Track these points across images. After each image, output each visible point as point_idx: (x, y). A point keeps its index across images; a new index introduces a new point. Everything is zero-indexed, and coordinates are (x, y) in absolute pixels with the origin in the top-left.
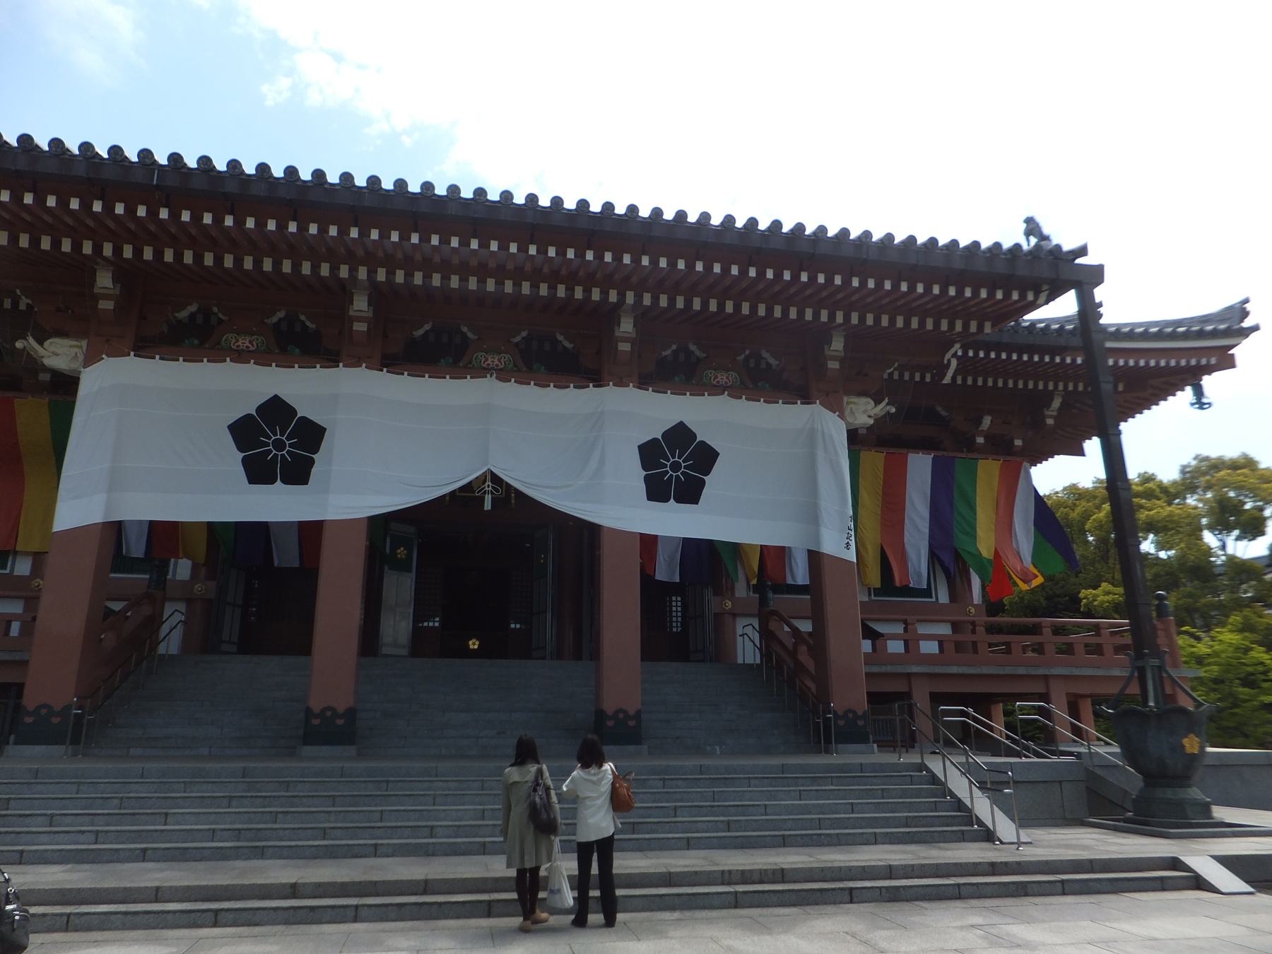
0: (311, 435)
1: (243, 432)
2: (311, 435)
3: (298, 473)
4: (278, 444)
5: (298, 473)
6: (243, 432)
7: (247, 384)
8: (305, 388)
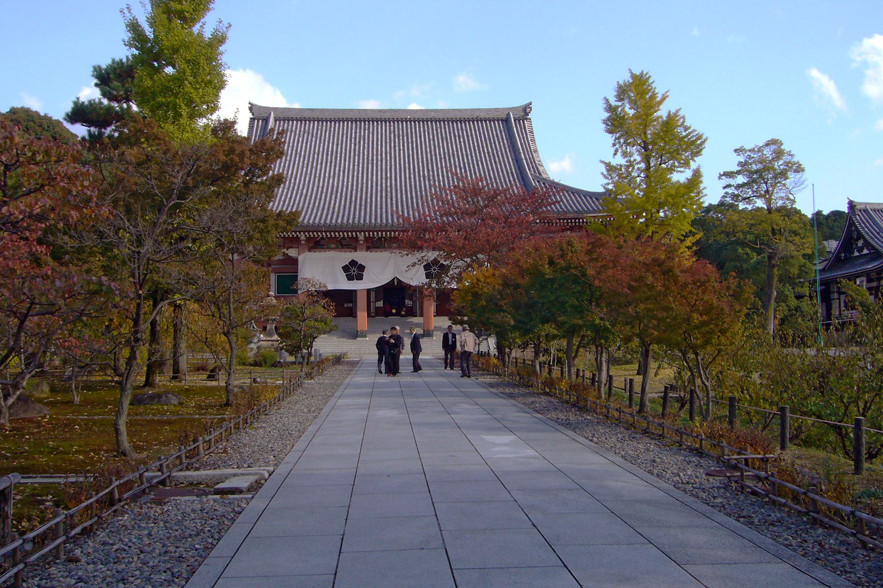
0: (362, 268)
1: (346, 269)
2: (362, 268)
3: (360, 277)
4: (354, 271)
5: (360, 277)
6: (346, 269)
7: (347, 257)
8: (360, 256)
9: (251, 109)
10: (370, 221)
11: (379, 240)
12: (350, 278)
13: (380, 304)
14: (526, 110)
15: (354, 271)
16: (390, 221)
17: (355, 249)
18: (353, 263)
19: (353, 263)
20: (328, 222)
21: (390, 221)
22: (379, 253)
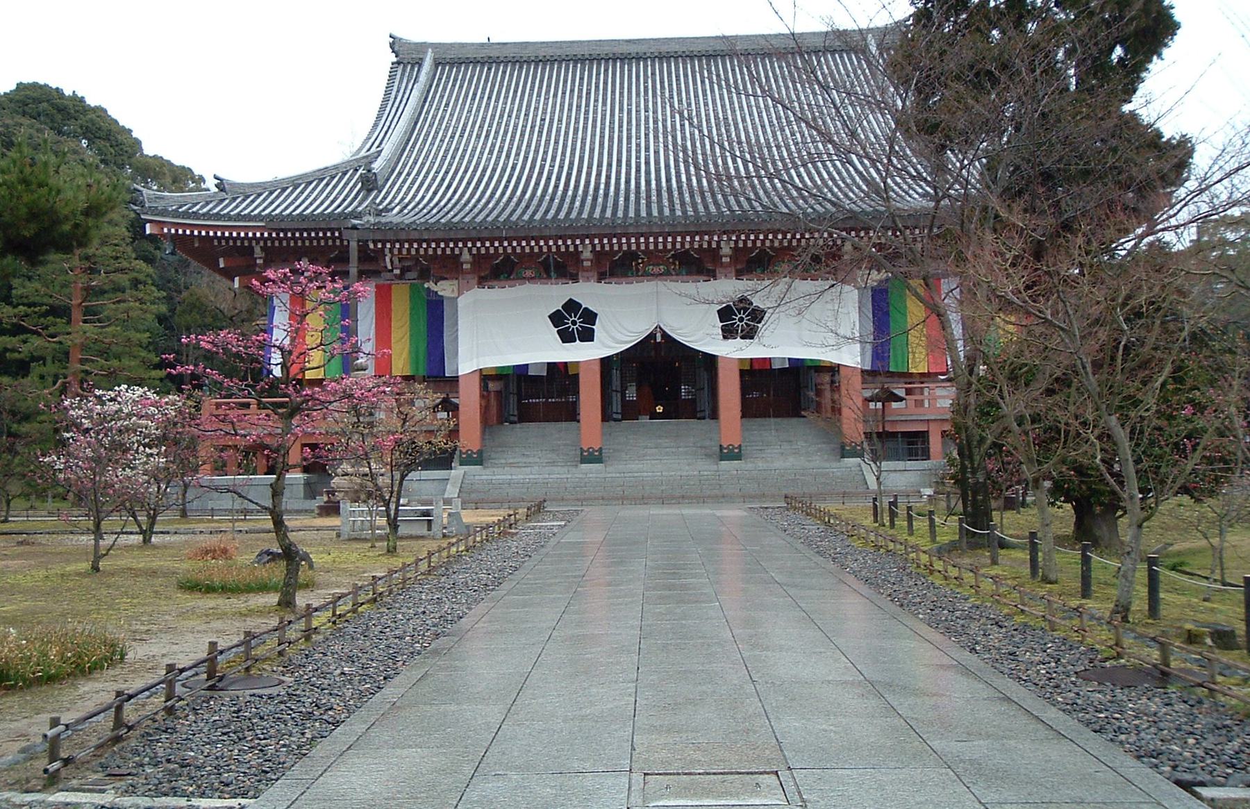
0: (590, 317)
2: (590, 317)
4: (739, 319)
5: (587, 336)
7: (556, 294)
8: (587, 293)
9: (392, 46)
10: (649, 213)
11: (625, 255)
12: (566, 337)
13: (632, 394)
14: (395, 44)
15: (574, 322)
16: (644, 214)
17: (575, 279)
18: (572, 306)
19: (572, 306)
20: (597, 215)
21: (644, 214)
22: (496, 290)
